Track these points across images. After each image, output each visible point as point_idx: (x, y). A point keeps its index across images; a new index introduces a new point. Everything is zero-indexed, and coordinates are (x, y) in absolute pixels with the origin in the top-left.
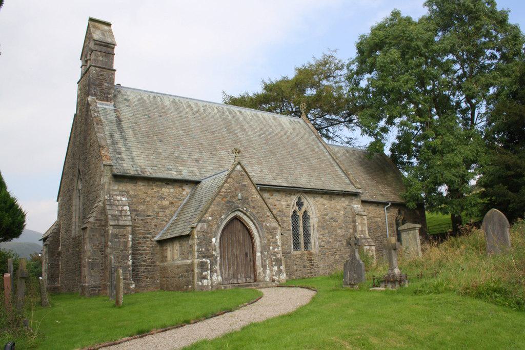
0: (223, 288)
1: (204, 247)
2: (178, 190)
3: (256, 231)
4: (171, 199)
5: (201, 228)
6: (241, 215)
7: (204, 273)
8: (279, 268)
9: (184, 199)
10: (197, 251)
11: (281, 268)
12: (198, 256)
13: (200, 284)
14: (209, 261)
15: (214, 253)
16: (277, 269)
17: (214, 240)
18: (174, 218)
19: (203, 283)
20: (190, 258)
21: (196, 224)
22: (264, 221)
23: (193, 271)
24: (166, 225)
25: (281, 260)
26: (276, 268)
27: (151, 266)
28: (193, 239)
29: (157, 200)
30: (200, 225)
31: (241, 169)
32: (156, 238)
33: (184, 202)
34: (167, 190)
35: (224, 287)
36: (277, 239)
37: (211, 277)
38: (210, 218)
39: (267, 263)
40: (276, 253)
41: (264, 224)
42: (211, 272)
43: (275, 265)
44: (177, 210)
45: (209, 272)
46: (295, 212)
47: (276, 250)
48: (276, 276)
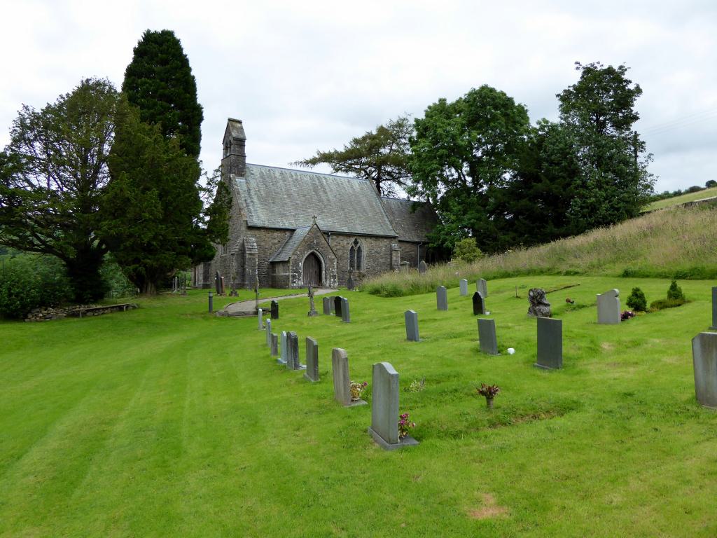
32: (270, 260)
46: (352, 247)
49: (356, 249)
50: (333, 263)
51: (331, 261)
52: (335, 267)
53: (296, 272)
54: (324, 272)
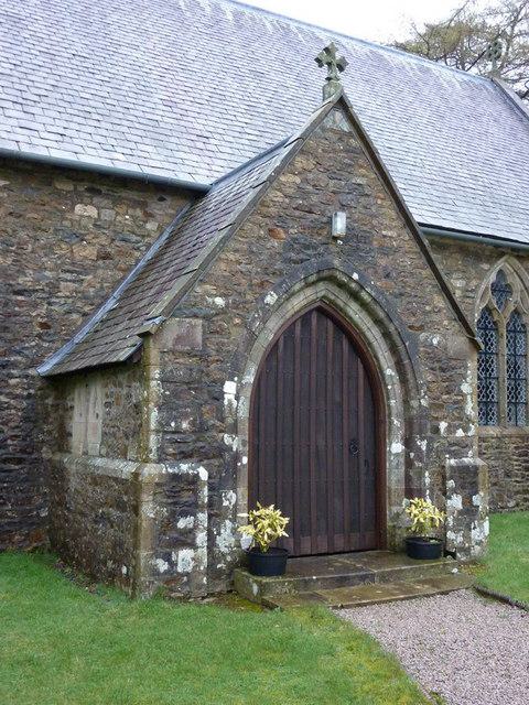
0: (255, 588)
1: (186, 416)
2: (126, 217)
3: (392, 363)
4: (103, 240)
5: (178, 340)
6: (341, 299)
7: (182, 524)
8: (467, 501)
9: (149, 246)
10: (157, 431)
11: (476, 500)
12: (161, 450)
13: (163, 566)
14: (203, 474)
15: (227, 439)
16: (460, 507)
17: (230, 388)
18: (111, 304)
19: (173, 564)
20: (131, 454)
21: (157, 321)
22: (421, 328)
23: (136, 509)
24: (83, 325)
25: (474, 471)
26: (456, 502)
27: (20, 461)
28: (145, 380)
29: (52, 239)
30: (174, 328)
31: (346, 127)
32: (44, 369)
33: (149, 255)
34: (92, 211)
35: (261, 585)
36: (464, 395)
37: (211, 539)
38: (220, 301)
39: (427, 481)
40: (459, 448)
41: (423, 336)
42: (210, 516)
43: (454, 491)
44: (123, 279)
45: (203, 517)
46: (488, 310)
47: (460, 433)
48: (456, 531)
49: (503, 318)
50: (452, 387)
51: (447, 368)
52: (471, 408)
53: (200, 455)
54: (397, 447)
